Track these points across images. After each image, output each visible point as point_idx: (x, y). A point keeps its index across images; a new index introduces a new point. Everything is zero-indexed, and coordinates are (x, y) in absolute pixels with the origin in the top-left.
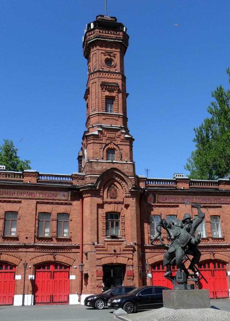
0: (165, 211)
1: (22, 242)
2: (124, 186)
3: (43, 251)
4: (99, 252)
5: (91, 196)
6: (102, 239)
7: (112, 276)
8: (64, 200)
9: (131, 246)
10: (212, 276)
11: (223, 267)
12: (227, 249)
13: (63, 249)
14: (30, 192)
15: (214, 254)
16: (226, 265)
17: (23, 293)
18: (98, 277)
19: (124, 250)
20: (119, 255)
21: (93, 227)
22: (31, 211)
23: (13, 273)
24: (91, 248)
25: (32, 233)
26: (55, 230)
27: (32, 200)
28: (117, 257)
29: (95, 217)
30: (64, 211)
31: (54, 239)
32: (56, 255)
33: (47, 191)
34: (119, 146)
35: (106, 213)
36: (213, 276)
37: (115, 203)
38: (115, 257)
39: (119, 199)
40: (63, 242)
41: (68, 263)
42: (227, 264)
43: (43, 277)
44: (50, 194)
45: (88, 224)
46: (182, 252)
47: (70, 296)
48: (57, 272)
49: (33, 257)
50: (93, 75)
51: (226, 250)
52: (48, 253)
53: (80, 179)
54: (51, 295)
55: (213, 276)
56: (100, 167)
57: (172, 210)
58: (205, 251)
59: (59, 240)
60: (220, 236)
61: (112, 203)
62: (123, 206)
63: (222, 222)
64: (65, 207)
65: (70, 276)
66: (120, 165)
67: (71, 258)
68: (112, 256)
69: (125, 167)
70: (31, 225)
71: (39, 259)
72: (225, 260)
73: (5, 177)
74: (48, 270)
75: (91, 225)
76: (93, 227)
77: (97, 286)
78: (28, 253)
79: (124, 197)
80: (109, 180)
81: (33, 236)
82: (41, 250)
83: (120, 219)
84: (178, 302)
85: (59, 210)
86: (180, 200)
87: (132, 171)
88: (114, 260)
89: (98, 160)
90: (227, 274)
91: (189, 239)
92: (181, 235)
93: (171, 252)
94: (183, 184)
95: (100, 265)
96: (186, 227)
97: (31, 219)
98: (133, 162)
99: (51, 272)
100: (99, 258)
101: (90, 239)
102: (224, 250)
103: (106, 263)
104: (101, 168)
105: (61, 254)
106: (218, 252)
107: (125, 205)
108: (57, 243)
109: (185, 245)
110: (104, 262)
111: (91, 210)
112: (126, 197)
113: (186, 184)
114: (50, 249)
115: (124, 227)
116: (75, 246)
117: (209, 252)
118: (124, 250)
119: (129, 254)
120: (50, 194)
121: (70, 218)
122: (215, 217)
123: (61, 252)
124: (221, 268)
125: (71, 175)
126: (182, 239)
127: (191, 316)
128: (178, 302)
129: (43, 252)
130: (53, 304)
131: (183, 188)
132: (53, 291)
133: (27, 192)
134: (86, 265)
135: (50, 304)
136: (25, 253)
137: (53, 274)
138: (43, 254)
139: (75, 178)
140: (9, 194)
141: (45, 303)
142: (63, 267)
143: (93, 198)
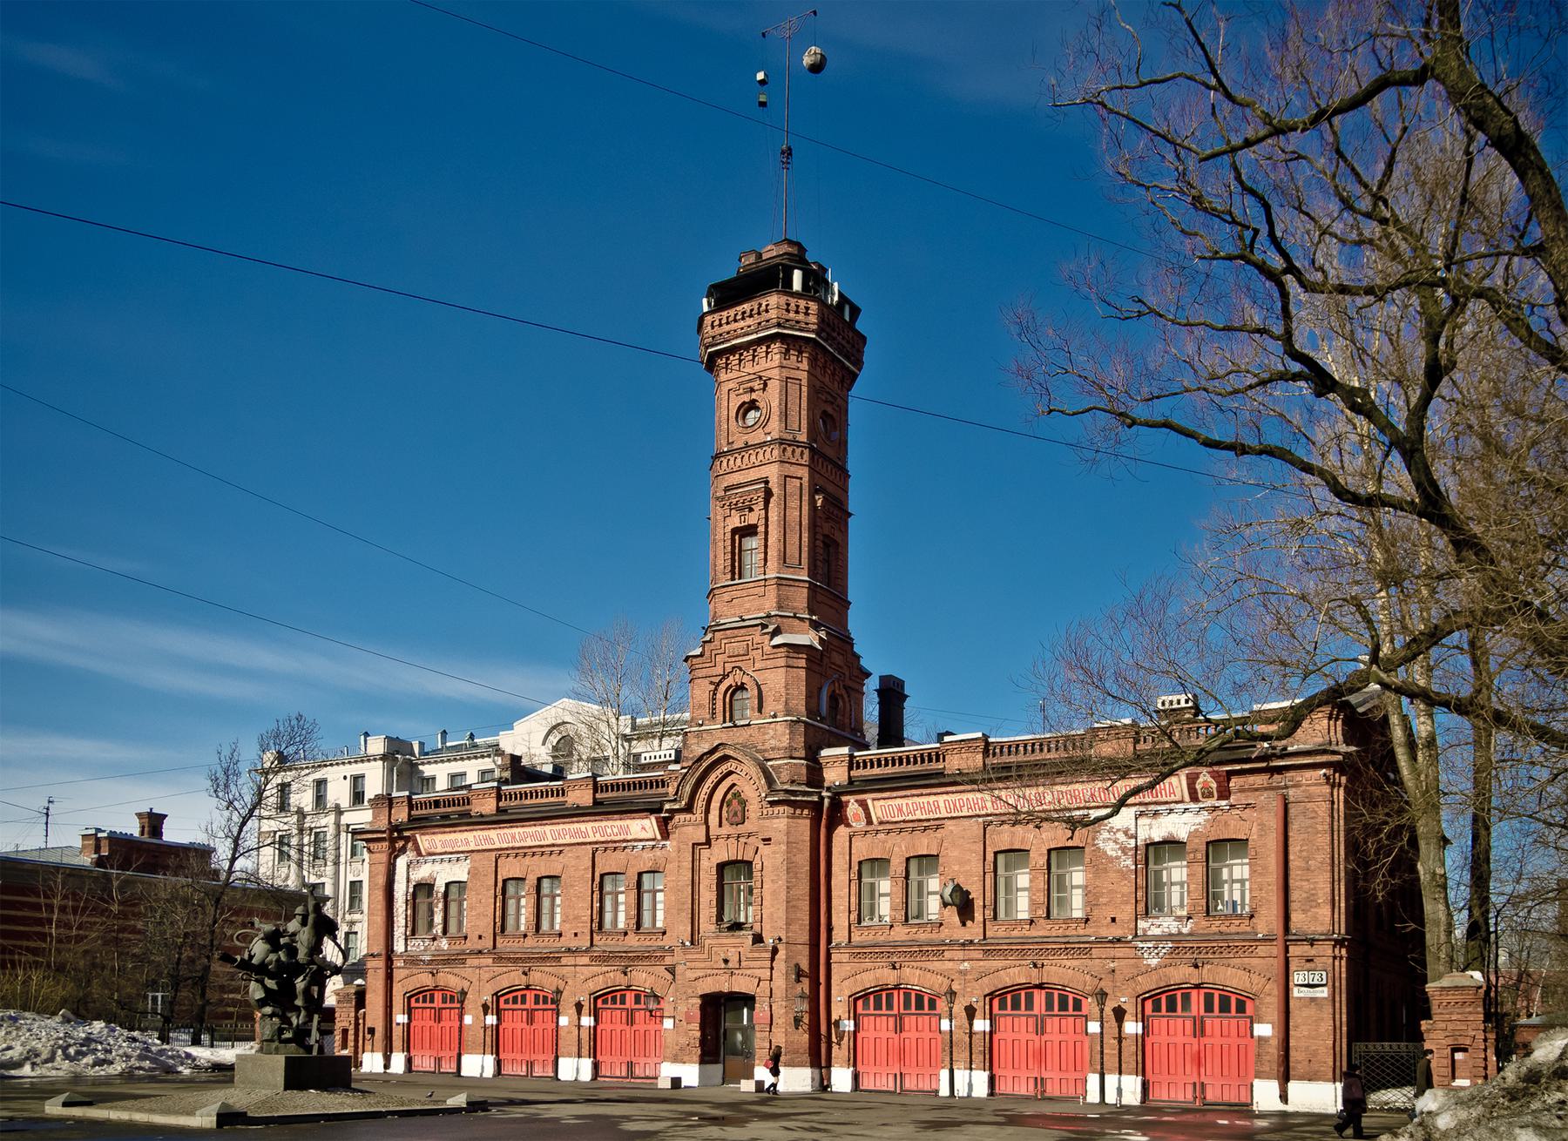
7: (745, 1023)
8: (647, 840)
43: (1171, 1032)
48: (538, 1010)
50: (732, 459)
57: (926, 841)
74: (622, 1006)
86: (942, 805)
99: (1037, 1016)
137: (1042, 1021)
140: (40, 922)
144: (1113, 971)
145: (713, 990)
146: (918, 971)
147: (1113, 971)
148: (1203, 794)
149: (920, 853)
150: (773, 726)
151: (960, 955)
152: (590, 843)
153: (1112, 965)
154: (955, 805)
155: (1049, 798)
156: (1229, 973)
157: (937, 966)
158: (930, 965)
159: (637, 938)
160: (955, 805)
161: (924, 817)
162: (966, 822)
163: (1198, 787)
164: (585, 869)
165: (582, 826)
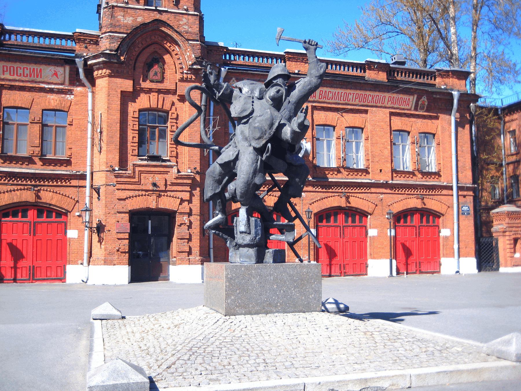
2: (173, 50)
5: (110, 76)
6: (132, 160)
9: (188, 177)
11: (360, 221)
12: (372, 189)
13: (54, 179)
15: (348, 198)
16: (367, 217)
18: (118, 234)
19: (173, 184)
20: (163, 194)
21: (112, 137)
24: (107, 178)
26: (37, 142)
28: (159, 196)
29: (115, 117)
31: (36, 160)
32: (39, 191)
33: (18, 64)
35: (140, 111)
37: (159, 91)
38: (154, 197)
39: (168, 85)
40: (54, 166)
41: (64, 206)
42: (369, 216)
44: (27, 69)
46: (253, 163)
51: (368, 191)
52: (22, 187)
53: (89, 43)
56: (131, 18)
59: (47, 162)
60: (361, 166)
61: (153, 92)
62: (175, 98)
63: (367, 139)
66: (171, 17)
68: (148, 195)
69: (182, 20)
72: (366, 209)
77: (118, 251)
79: (177, 81)
82: (9, 181)
83: (169, 124)
84: (233, 298)
87: (196, 29)
88: (151, 202)
89: (127, 3)
91: (276, 124)
92: (254, 115)
93: (225, 162)
94: (298, 63)
95: (124, 210)
96: (270, 94)
98: (200, 12)
100: (122, 197)
102: (366, 191)
107: (179, 96)
108: (43, 167)
109: (264, 142)
111: (109, 104)
112: (182, 80)
113: (303, 64)
114: (17, 179)
116: (78, 173)
118: (173, 184)
119: (184, 193)
121: (69, 119)
122: (354, 129)
123: (48, 186)
124: (357, 223)
125: (71, 34)
126: (257, 125)
127: (261, 338)
128: (233, 298)
129: (12, 185)
131: (296, 72)
132: (35, 259)
134: (97, 211)
138: (12, 188)
139: (79, 40)
141: (55, 279)
142: (54, 214)
143: (113, 79)
148: (420, 107)
150: (186, 16)
163: (420, 103)
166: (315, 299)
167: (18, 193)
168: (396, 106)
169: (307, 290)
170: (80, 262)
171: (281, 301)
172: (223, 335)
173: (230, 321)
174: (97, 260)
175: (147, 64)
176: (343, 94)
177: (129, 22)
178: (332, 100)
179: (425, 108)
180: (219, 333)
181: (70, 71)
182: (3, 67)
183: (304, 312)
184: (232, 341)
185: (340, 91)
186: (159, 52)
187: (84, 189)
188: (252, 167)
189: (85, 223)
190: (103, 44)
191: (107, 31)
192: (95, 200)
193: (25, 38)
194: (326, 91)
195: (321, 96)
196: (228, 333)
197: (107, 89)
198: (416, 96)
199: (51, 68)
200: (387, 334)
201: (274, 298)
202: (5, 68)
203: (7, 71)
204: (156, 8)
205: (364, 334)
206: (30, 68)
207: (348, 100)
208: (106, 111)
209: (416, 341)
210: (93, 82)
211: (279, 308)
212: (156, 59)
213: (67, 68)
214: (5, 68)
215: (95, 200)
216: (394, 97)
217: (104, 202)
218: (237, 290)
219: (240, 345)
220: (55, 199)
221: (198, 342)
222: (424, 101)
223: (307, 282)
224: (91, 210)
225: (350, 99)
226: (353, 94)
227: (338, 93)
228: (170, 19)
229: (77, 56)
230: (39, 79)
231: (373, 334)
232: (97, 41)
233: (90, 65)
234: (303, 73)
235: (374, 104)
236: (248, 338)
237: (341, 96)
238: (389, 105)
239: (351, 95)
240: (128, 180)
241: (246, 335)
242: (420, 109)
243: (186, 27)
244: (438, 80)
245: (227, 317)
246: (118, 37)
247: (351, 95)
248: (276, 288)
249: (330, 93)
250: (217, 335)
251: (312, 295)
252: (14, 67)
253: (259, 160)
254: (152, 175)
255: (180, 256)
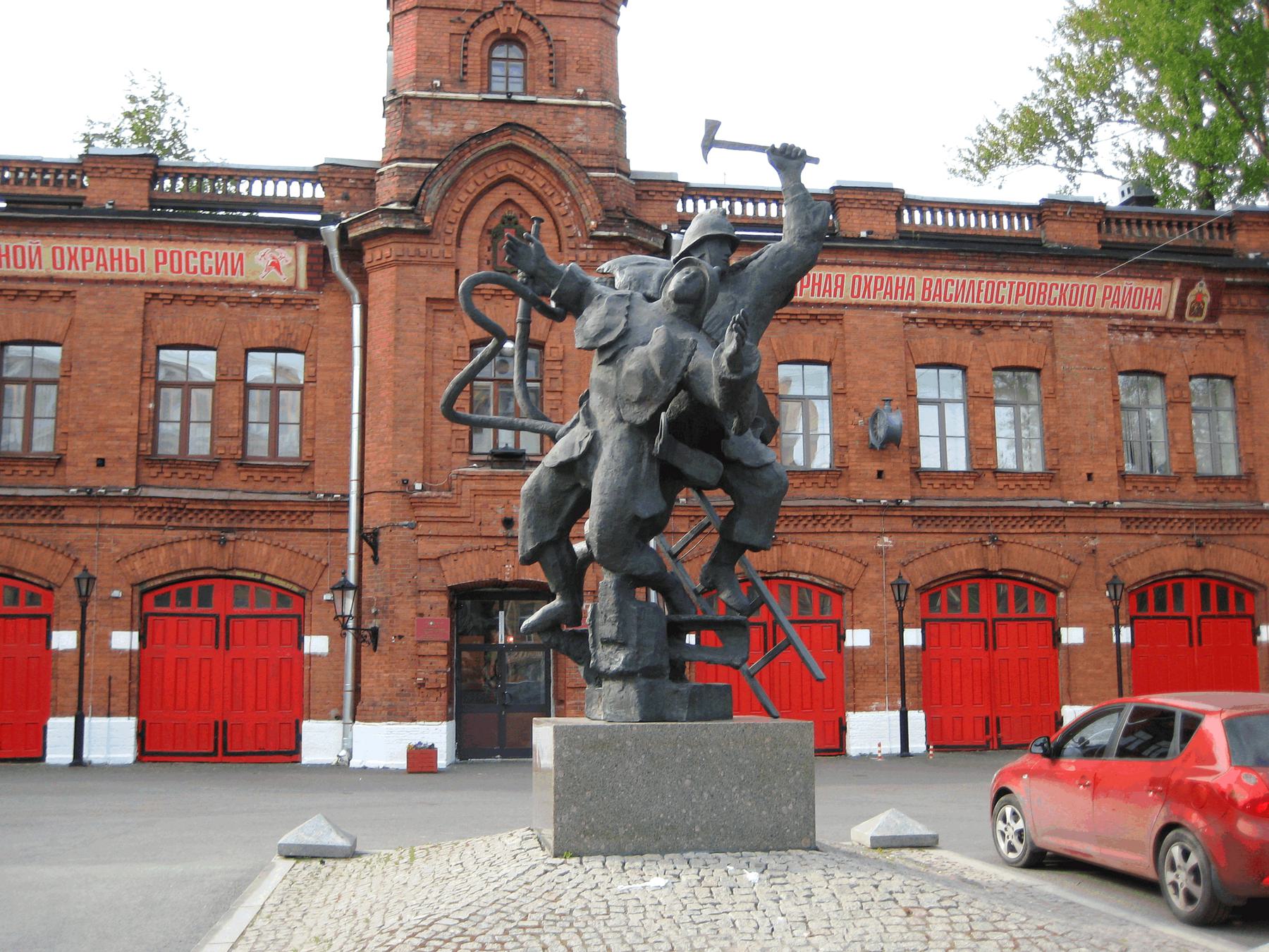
0: (774, 342)
1: (79, 475)
3: (175, 524)
4: (433, 529)
10: (1191, 641)
14: (112, 251)
17: (75, 710)
22: (122, 338)
23: (44, 621)
25: (126, 438)
27: (123, 288)
30: (277, 340)
34: (545, 22)
36: (1195, 643)
44: (210, 256)
45: (383, 394)
47: (307, 726)
49: (131, 550)
51: (1057, 530)
52: (198, 533)
54: (216, 723)
55: (1195, 643)
56: (450, 125)
58: (1251, 535)
64: (284, 319)
65: (307, 639)
67: (311, 555)
69: (572, 122)
70: (122, 404)
71: (158, 560)
73: (1206, 321)
75: (395, 402)
76: (406, 411)
77: (421, 685)
78: (106, 533)
80: (534, 193)
81: (128, 455)
82: (170, 518)
84: (574, 810)
85: (256, 336)
90: (1060, 639)
97: (120, 373)
99: (217, 618)
100: (431, 555)
101: (390, 465)
102: (1052, 529)
103: (465, 579)
104: (454, 130)
105: (260, 539)
106: (1024, 539)
110: (457, 575)
111: (397, 330)
115: (561, 411)
116: (329, 499)
117: (978, 538)
120: (195, 256)
130: (226, 759)
131: (863, 234)
133: (101, 250)
134: (372, 590)
135: (214, 758)
136: (91, 532)
137: (994, 628)
144: (1094, 551)
145: (477, 579)
146: (810, 550)
147: (1094, 551)
148: (1192, 310)
149: (801, 357)
150: (581, 112)
151: (877, 524)
152: (141, 283)
153: (1092, 543)
154: (868, 286)
155: (1004, 292)
156: (1234, 555)
157: (841, 541)
158: (828, 541)
159: (244, 476)
160: (868, 286)
161: (815, 298)
162: (881, 316)
163: (1190, 299)
164: (127, 333)
165: (135, 249)
166: (797, 816)
167: (189, 546)
168: (1126, 310)
169: (774, 792)
170: (334, 712)
171: (704, 822)
172: (523, 909)
173: (564, 868)
174: (371, 708)
175: (489, 232)
176: (983, 287)
177: (446, 134)
178: (956, 300)
179: (1205, 311)
180: (516, 904)
181: (309, 256)
182: (157, 252)
183: (767, 850)
184: (540, 926)
185: (977, 277)
186: (518, 201)
187: (343, 536)
188: (625, 474)
189: (341, 619)
190: (384, 189)
191: (393, 157)
192: (368, 562)
193: (257, 185)
194: (939, 281)
195: (927, 292)
196: (540, 903)
197: (393, 295)
198: (1177, 283)
199: (265, 251)
200: (968, 916)
201: (684, 811)
202: (161, 254)
203: (165, 262)
204: (509, 97)
205: (904, 914)
206: (217, 254)
207: (997, 301)
208: (392, 349)
209: (1044, 937)
210: (361, 278)
211: (699, 839)
212: (510, 219)
213: (303, 249)
214: (161, 254)
215: (368, 562)
216: (1118, 288)
217: (387, 567)
218: (586, 790)
219: (554, 937)
220: (276, 560)
221: (449, 926)
222: (1200, 295)
223: (775, 771)
224: (358, 588)
225: (1003, 297)
226: (1012, 283)
227: (972, 282)
228: (544, 121)
229: (326, 220)
230: (238, 279)
231: (930, 915)
232: (373, 181)
233: (355, 238)
234: (881, 237)
235: (1068, 307)
236: (586, 918)
237: (980, 291)
238: (1108, 308)
239: (1005, 286)
240: (446, 512)
241: (586, 908)
242: (1190, 315)
243: (582, 138)
244: (1241, 238)
245: (559, 860)
246: (419, 170)
247: (1005, 286)
248: (691, 786)
249: (950, 283)
250: (509, 909)
251: (787, 805)
252: (23, 248)
253: (646, 455)
254: (505, 499)
255: (575, 699)
